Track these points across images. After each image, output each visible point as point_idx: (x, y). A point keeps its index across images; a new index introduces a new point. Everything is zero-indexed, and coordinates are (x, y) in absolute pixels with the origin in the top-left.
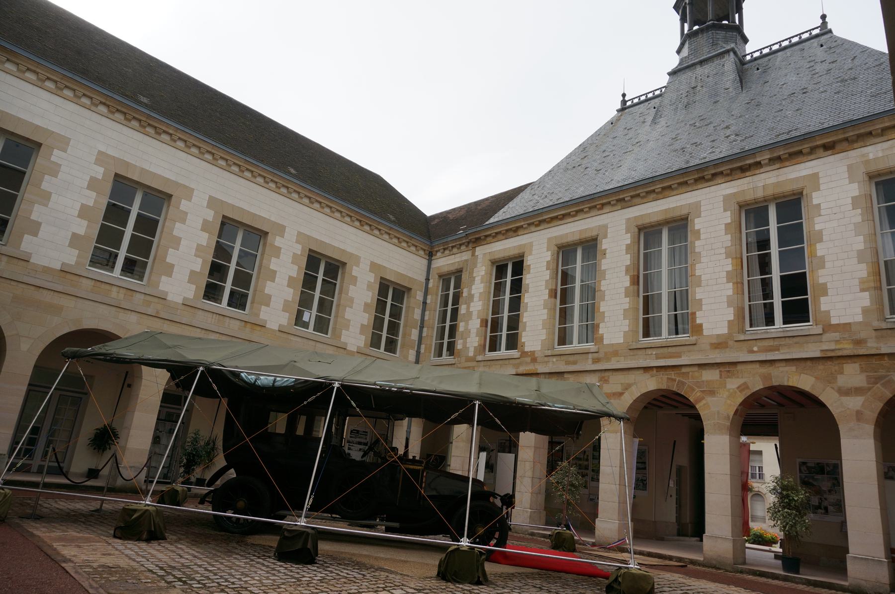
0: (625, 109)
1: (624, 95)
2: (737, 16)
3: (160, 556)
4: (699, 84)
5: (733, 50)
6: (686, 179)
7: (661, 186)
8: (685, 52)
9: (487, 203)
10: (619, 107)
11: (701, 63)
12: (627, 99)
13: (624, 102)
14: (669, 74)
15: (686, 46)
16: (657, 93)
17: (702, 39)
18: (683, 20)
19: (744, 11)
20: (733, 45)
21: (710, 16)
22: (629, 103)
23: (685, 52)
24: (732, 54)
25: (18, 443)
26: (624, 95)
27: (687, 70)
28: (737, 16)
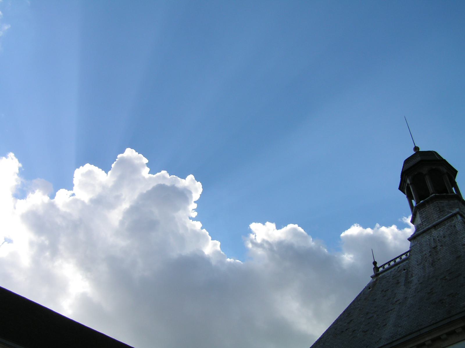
0: (379, 274)
1: (375, 263)
2: (453, 189)
3: (462, 304)
4: (439, 244)
5: (458, 213)
6: (453, 328)
7: (430, 338)
8: (418, 220)
9: (460, 196)
10: (373, 273)
11: (435, 227)
12: (378, 265)
13: (376, 269)
14: (371, 277)
15: (418, 216)
16: (404, 257)
17: (430, 209)
18: (410, 198)
19: (458, 184)
20: (457, 210)
21: (431, 190)
22: (381, 269)
23: (418, 220)
24: (459, 216)
25: (437, 156)
26: (375, 263)
27: (424, 234)
28: (453, 189)
